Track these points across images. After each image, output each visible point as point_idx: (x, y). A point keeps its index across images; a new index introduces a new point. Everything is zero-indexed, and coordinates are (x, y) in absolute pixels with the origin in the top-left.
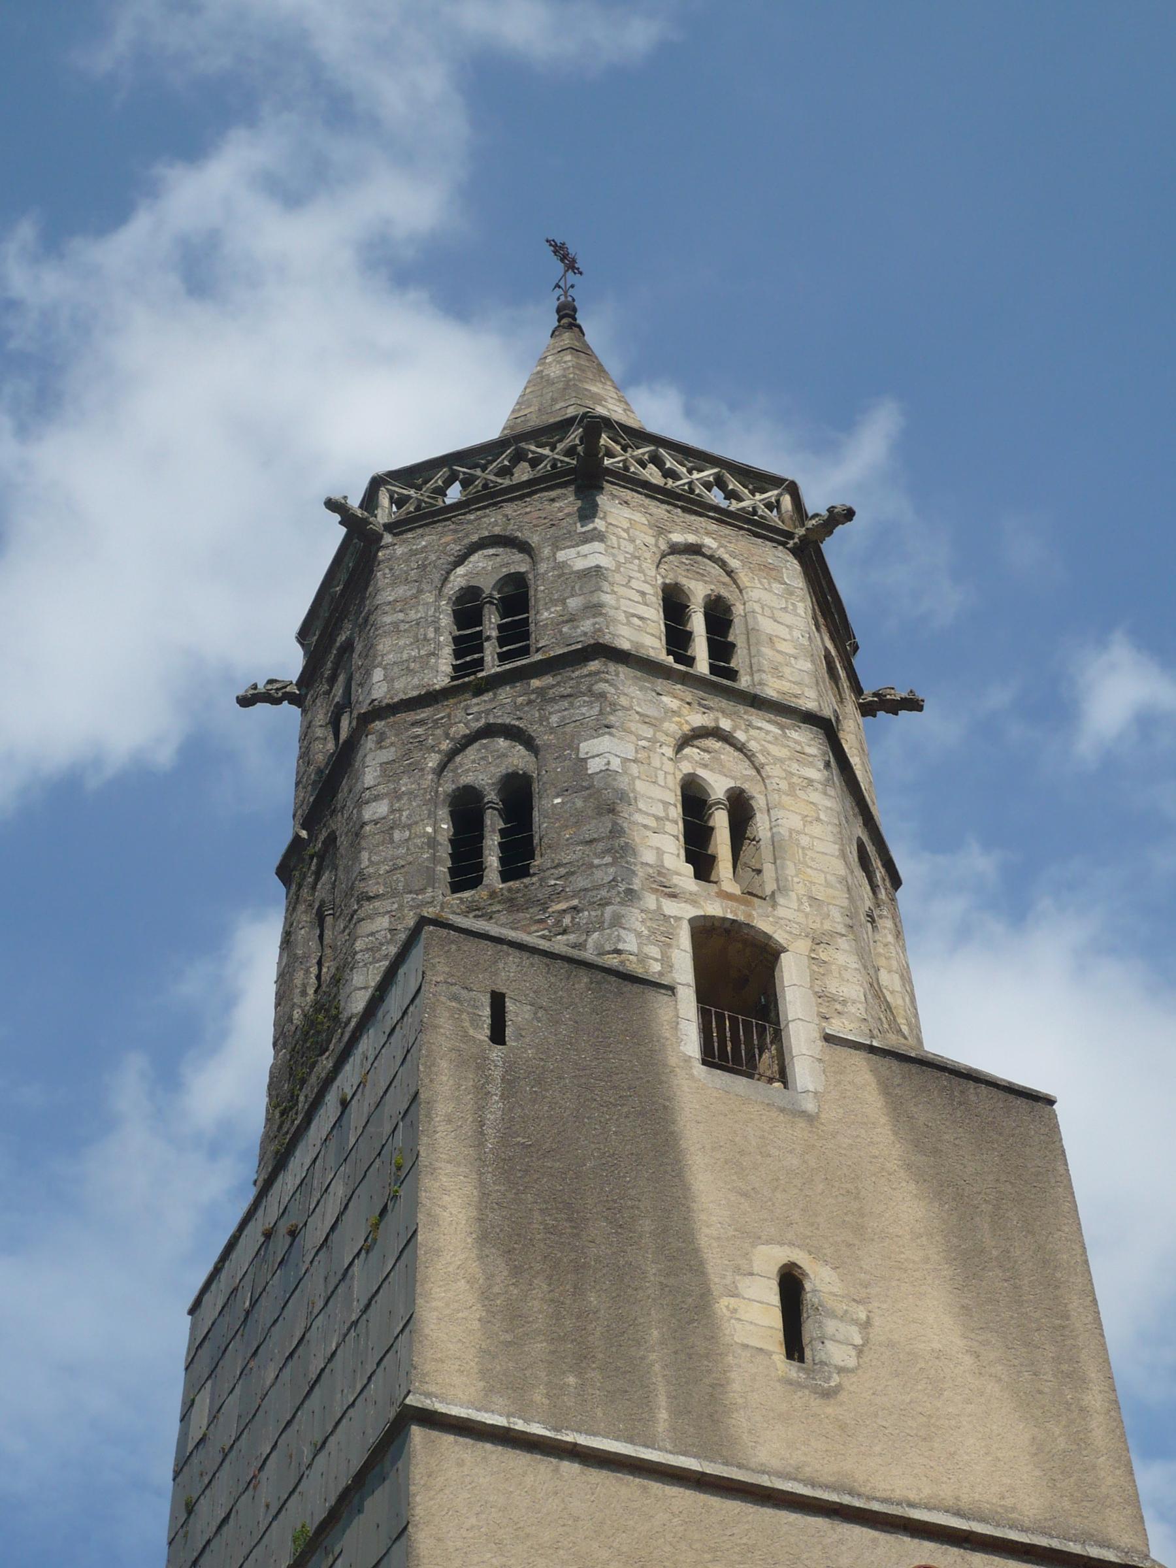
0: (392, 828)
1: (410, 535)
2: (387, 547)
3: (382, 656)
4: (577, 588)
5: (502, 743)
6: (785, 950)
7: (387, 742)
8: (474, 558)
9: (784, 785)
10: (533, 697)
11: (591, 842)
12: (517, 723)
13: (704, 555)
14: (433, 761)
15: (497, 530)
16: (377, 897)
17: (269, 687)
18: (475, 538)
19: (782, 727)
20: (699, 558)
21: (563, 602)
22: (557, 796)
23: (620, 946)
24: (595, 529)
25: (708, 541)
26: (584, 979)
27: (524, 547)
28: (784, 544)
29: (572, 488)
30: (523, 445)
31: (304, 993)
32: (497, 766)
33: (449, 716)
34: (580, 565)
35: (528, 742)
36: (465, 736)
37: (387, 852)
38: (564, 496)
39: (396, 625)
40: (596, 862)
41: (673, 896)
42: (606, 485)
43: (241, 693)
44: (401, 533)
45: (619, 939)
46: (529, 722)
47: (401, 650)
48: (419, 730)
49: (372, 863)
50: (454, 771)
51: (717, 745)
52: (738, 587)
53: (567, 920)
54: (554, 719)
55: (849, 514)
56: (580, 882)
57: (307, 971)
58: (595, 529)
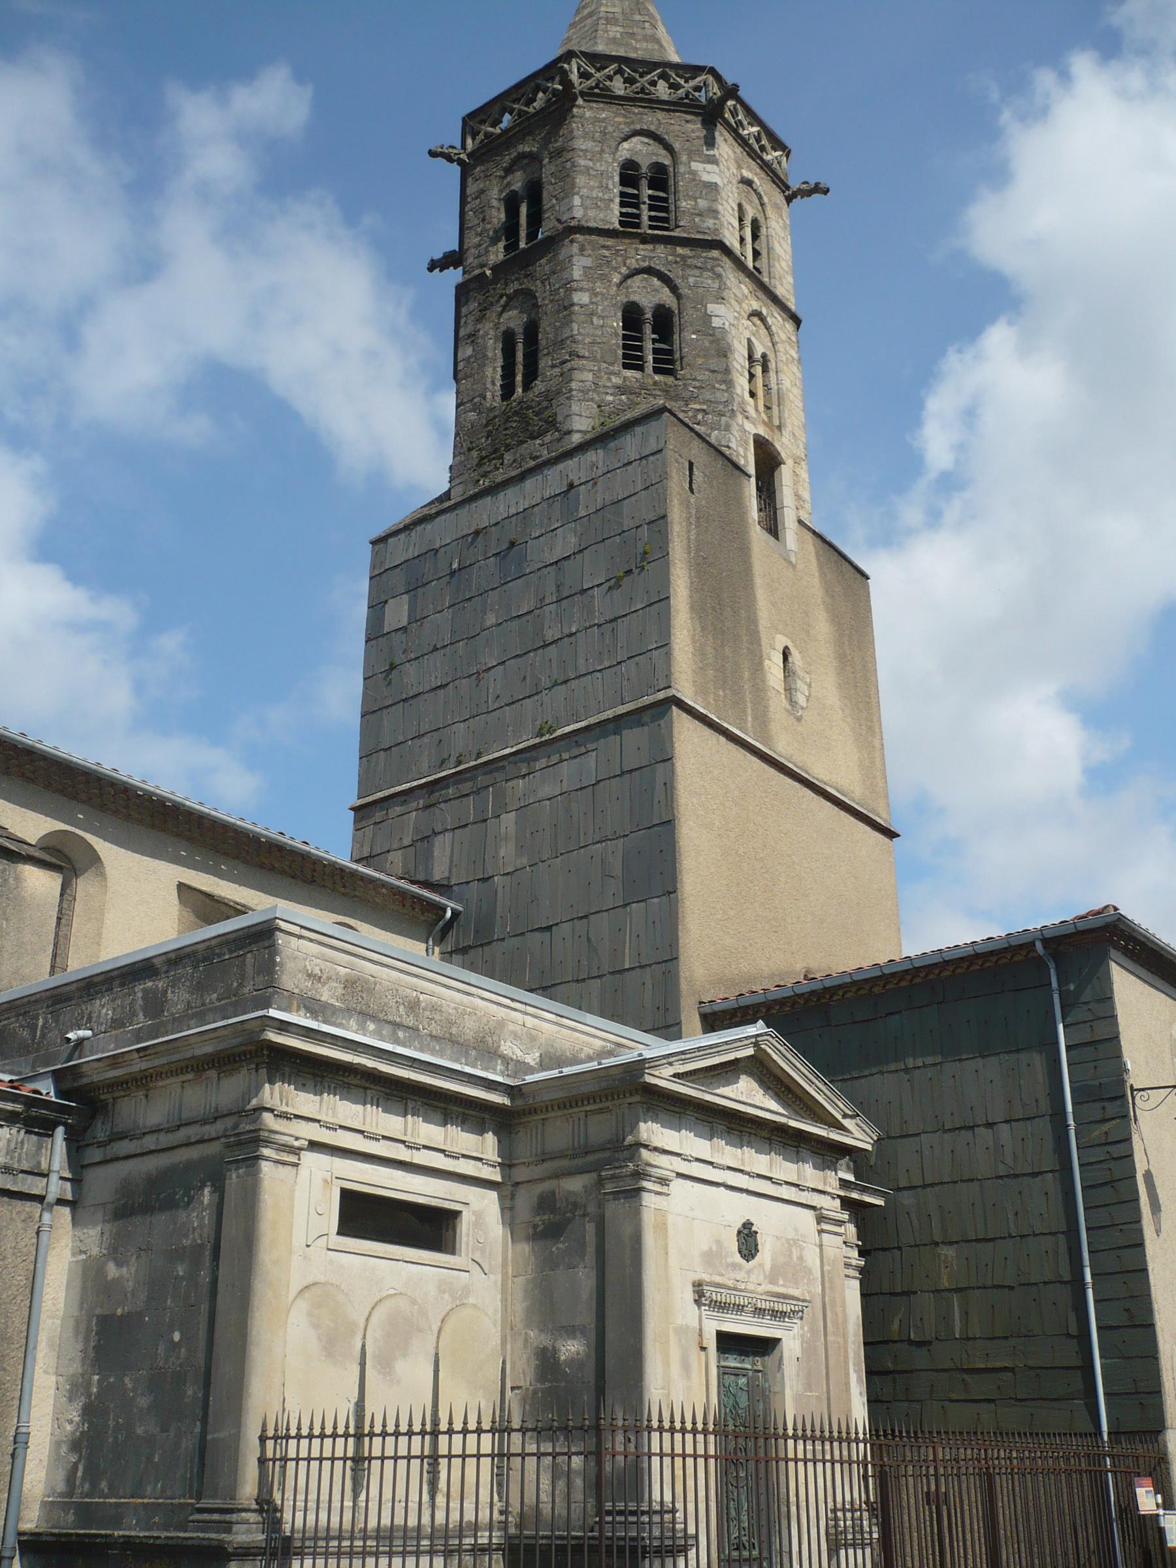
0: (592, 314)
1: (594, 105)
2: (579, 107)
3: (580, 188)
4: (704, 192)
5: (656, 281)
6: (784, 463)
7: (585, 253)
8: (635, 139)
9: (784, 359)
10: (678, 259)
11: (714, 371)
12: (669, 274)
13: (752, 188)
14: (616, 279)
15: (653, 128)
16: (583, 357)
17: (451, 150)
18: (638, 127)
19: (783, 320)
20: (750, 189)
21: (695, 199)
22: (694, 333)
23: (730, 445)
24: (714, 156)
25: (756, 180)
26: (720, 462)
27: (669, 148)
28: (784, 192)
29: (700, 118)
30: (667, 70)
31: (493, 383)
32: (654, 296)
33: (626, 250)
34: (706, 178)
35: (674, 289)
36: (635, 269)
37: (588, 329)
38: (694, 123)
39: (588, 168)
40: (717, 386)
41: (747, 418)
42: (718, 125)
43: (433, 148)
44: (590, 101)
45: (729, 440)
46: (675, 274)
47: (592, 189)
48: (607, 253)
49: (580, 334)
50: (627, 288)
51: (758, 322)
52: (765, 215)
53: (700, 417)
54: (691, 280)
55: (826, 191)
56: (707, 395)
57: (494, 368)
58: (714, 156)
